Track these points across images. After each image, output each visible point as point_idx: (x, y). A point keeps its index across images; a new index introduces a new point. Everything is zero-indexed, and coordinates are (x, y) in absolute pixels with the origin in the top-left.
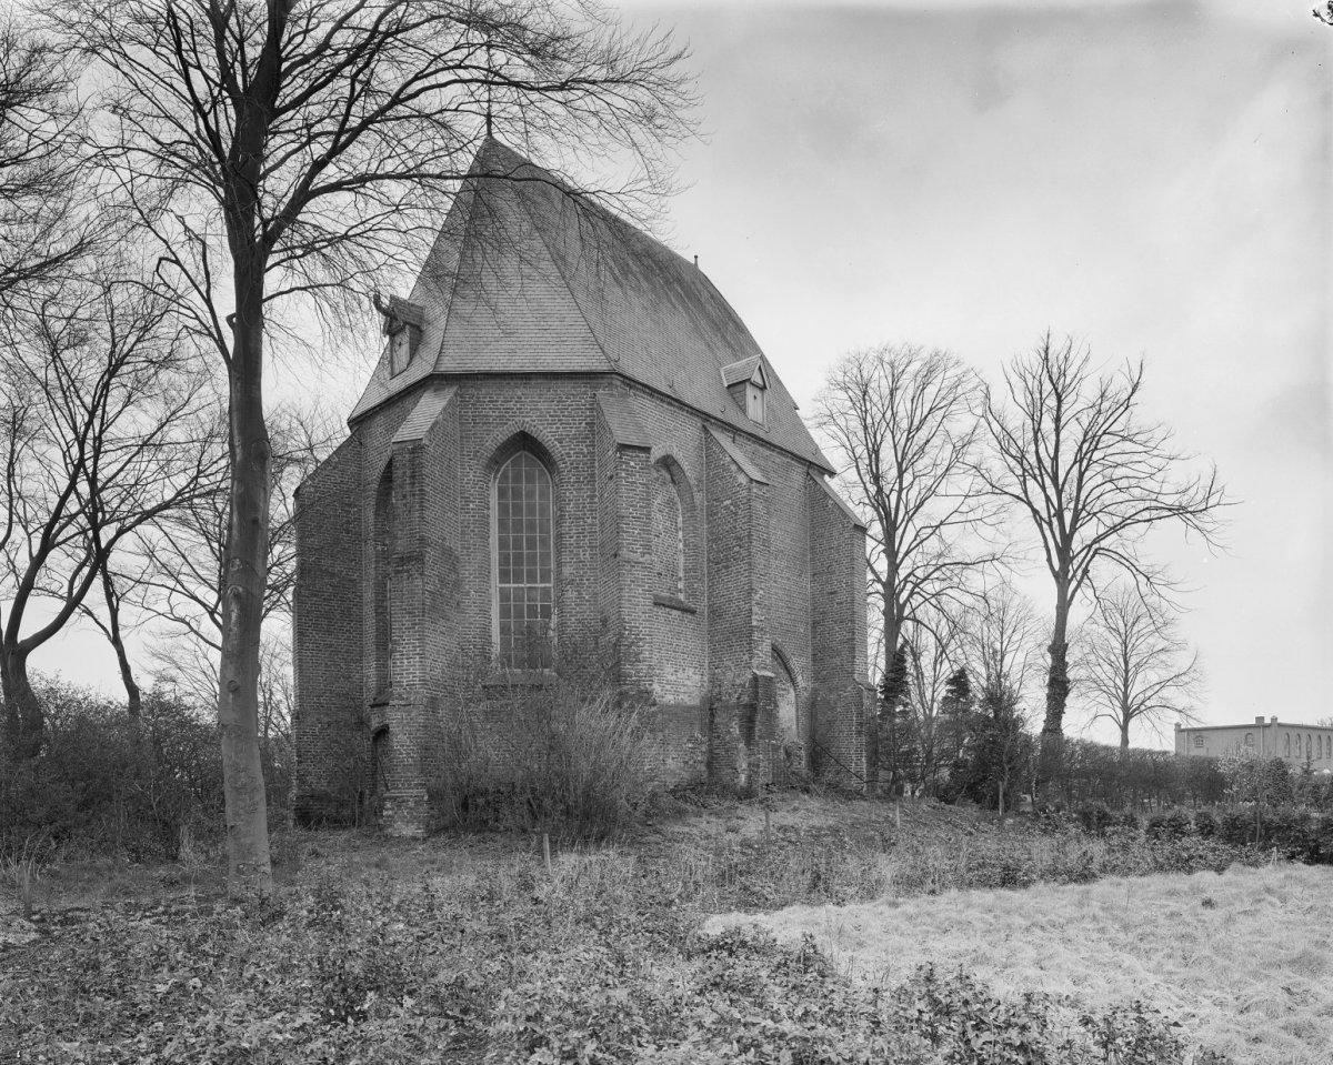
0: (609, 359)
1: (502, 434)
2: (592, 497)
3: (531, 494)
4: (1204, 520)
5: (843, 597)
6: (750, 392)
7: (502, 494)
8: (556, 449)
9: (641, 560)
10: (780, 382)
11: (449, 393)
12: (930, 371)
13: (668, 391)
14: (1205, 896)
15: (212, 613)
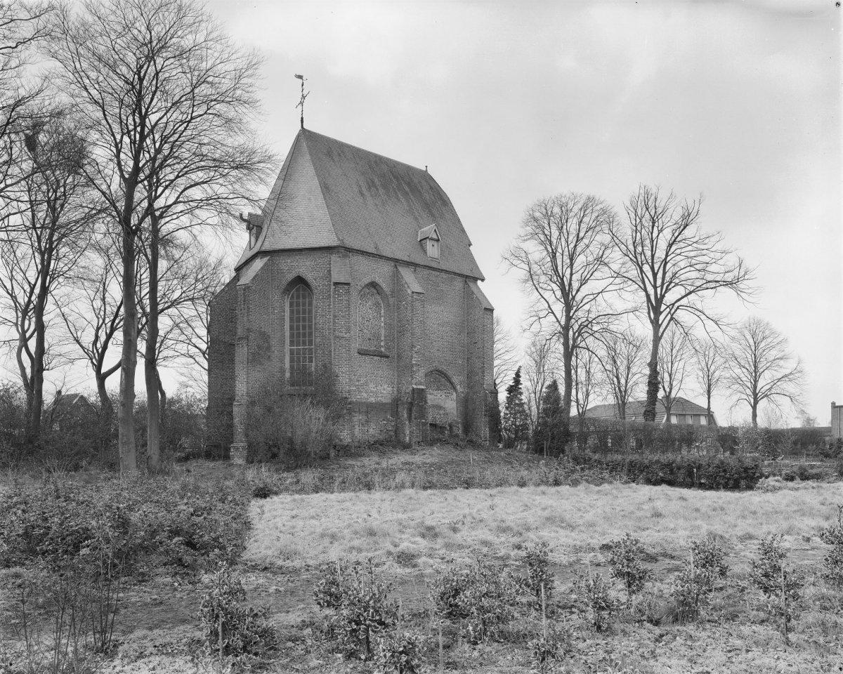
0: (339, 239)
1: (290, 277)
2: (329, 305)
3: (304, 304)
4: (741, 285)
5: (479, 345)
6: (429, 244)
7: (291, 305)
8: (313, 283)
9: (345, 336)
10: (463, 231)
11: (266, 259)
12: (584, 208)
13: (373, 251)
14: (684, 504)
15: (204, 353)
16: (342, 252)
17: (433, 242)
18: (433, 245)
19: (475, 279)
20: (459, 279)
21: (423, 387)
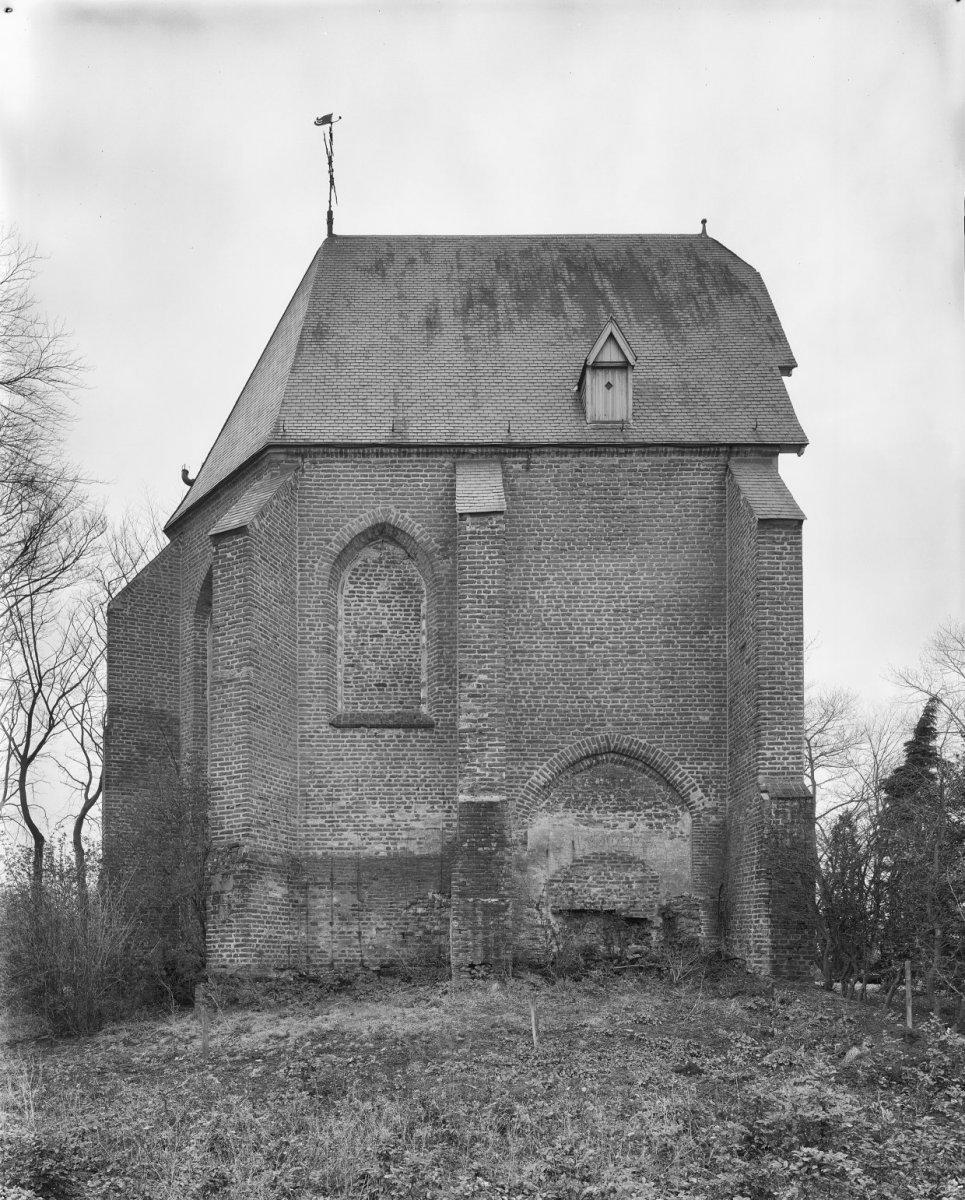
9: (237, 675)
16: (279, 463)
17: (610, 377)
18: (609, 386)
19: (767, 452)
20: (701, 462)
21: (495, 798)
